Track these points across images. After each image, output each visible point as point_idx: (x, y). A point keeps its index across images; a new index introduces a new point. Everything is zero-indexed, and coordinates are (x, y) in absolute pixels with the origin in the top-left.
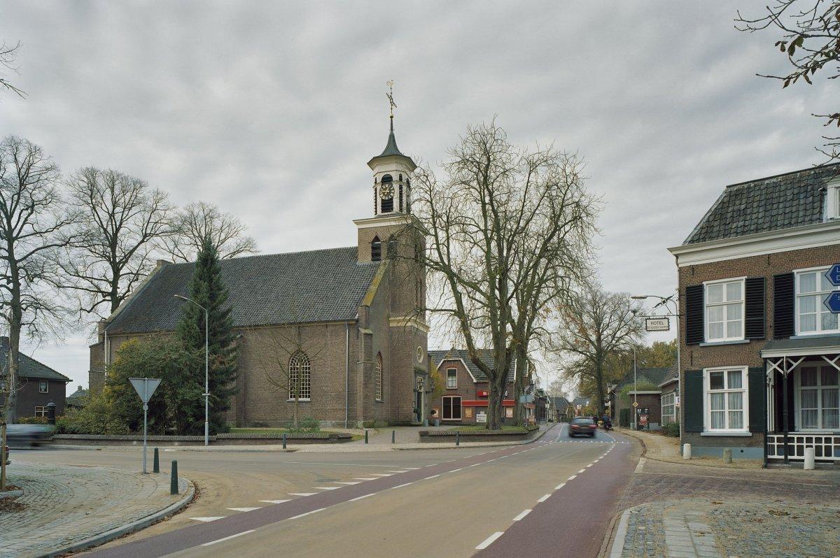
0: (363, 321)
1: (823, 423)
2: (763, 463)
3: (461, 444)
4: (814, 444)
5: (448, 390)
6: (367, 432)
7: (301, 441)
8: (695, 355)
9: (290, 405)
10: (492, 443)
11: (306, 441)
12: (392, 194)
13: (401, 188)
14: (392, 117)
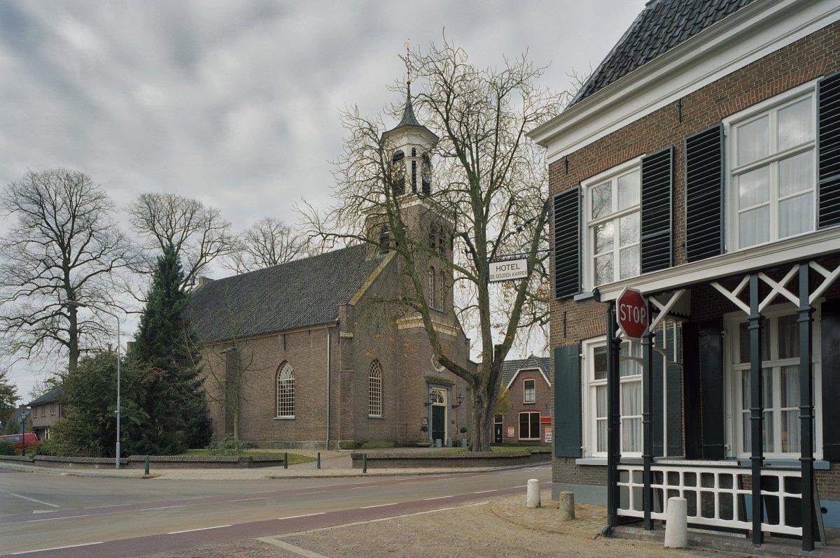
0: (344, 322)
1: (784, 442)
2: (603, 525)
3: (370, 471)
4: (681, 487)
5: (525, 404)
6: (319, 454)
7: (208, 465)
8: (570, 318)
9: (277, 423)
10: (450, 470)
11: (213, 465)
12: (403, 173)
13: (414, 164)
14: (409, 83)
